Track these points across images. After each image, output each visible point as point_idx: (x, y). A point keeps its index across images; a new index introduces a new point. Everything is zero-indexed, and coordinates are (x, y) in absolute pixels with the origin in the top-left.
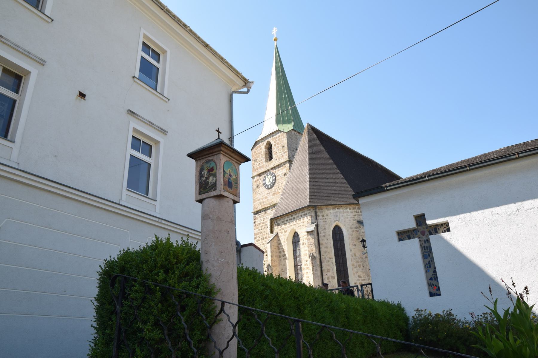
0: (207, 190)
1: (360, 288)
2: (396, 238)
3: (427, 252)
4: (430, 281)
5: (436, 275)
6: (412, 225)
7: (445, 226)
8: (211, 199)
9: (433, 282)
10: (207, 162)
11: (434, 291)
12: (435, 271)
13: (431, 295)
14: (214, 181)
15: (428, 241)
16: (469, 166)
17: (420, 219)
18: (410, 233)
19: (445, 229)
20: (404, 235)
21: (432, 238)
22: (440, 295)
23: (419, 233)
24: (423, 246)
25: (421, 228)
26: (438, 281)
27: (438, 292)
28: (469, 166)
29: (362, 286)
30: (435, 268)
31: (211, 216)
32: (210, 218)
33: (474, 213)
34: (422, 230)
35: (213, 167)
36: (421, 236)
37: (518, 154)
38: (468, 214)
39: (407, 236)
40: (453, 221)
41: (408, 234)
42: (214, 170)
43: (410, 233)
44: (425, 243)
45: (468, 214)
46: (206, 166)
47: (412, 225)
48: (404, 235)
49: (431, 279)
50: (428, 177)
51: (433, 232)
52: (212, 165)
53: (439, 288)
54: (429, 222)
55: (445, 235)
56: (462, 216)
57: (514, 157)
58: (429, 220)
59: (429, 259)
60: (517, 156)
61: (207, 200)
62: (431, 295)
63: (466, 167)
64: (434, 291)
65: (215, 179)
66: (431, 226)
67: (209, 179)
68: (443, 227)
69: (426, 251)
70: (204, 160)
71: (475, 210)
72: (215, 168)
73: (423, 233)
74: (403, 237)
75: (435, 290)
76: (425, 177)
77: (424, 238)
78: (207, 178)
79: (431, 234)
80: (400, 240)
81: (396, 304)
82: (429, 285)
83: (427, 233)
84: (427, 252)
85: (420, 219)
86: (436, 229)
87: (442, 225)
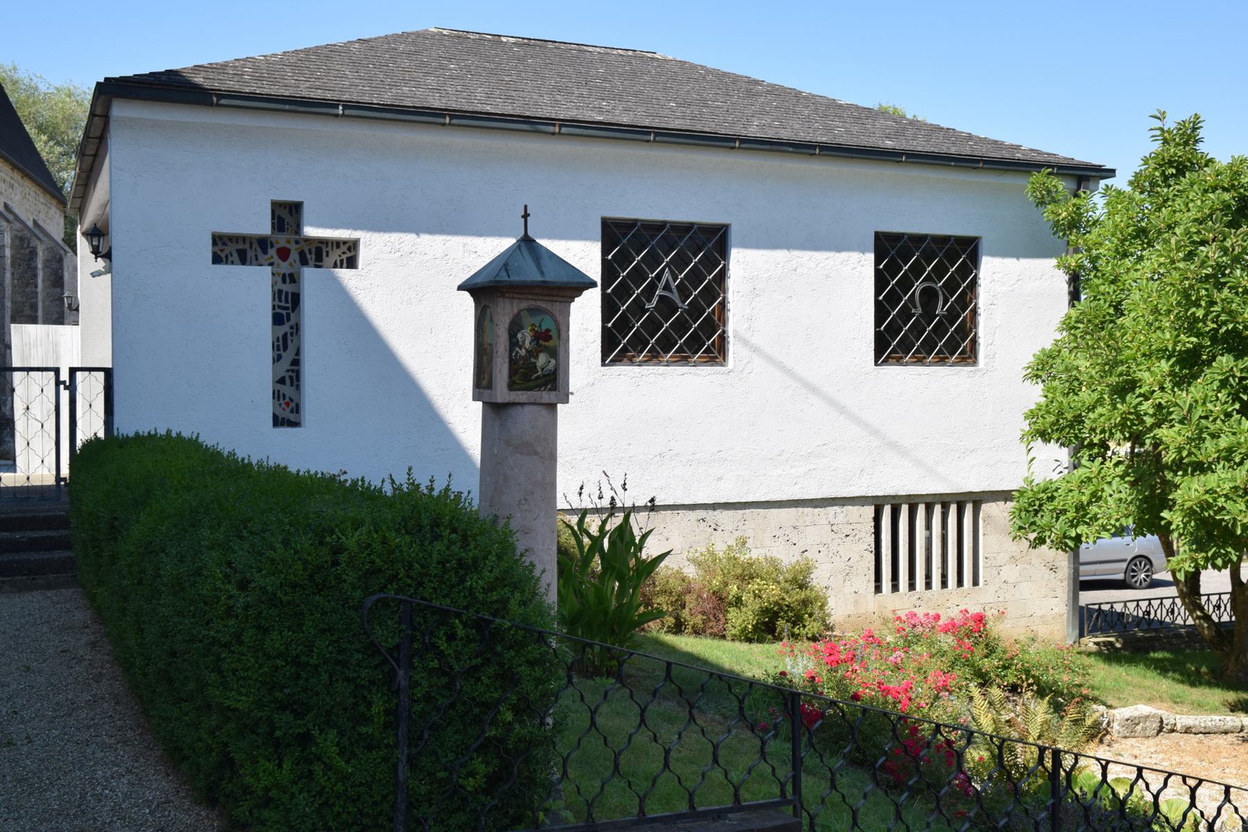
0: (531, 384)
1: (65, 376)
2: (207, 250)
3: (287, 308)
4: (279, 387)
5: (298, 373)
6: (263, 227)
7: (344, 248)
8: (541, 408)
9: (287, 390)
10: (533, 311)
11: (287, 414)
12: (296, 362)
13: (278, 422)
14: (551, 366)
15: (293, 279)
16: (452, 117)
17: (287, 214)
18: (247, 246)
19: (344, 257)
20: (231, 249)
21: (309, 275)
22: (296, 424)
23: (272, 252)
24: (276, 288)
25: (282, 240)
26: (298, 387)
27: (292, 417)
28: (452, 117)
29: (73, 371)
30: (298, 353)
31: (539, 449)
32: (536, 453)
33: (425, 238)
34: (282, 244)
35: (548, 331)
36: (276, 259)
37: (561, 126)
38: (413, 236)
39: (238, 251)
40: (372, 245)
41: (241, 246)
42: (551, 337)
43: (247, 246)
44: (284, 281)
45: (410, 237)
46: (528, 321)
47: (263, 227)
48: (231, 249)
49: (281, 381)
50: (345, 107)
51: (311, 258)
52: (547, 324)
53: (298, 406)
54: (310, 231)
55: (344, 274)
56: (395, 236)
57: (551, 129)
58: (312, 225)
59: (286, 328)
60: (557, 130)
61: (528, 408)
62: (278, 422)
63: (444, 116)
64: (287, 414)
65: (553, 361)
66: (309, 240)
67: (537, 358)
68: (339, 252)
69: (283, 304)
70: (524, 305)
71: (431, 232)
72: (553, 333)
73: (284, 254)
74: (227, 251)
75: (288, 410)
76: (336, 107)
77: (285, 267)
78: (533, 354)
79: (304, 262)
80: (217, 259)
81: (226, 454)
82: (277, 395)
83: (294, 256)
84: (287, 308)
85: (287, 214)
86: (319, 252)
87: (338, 243)
